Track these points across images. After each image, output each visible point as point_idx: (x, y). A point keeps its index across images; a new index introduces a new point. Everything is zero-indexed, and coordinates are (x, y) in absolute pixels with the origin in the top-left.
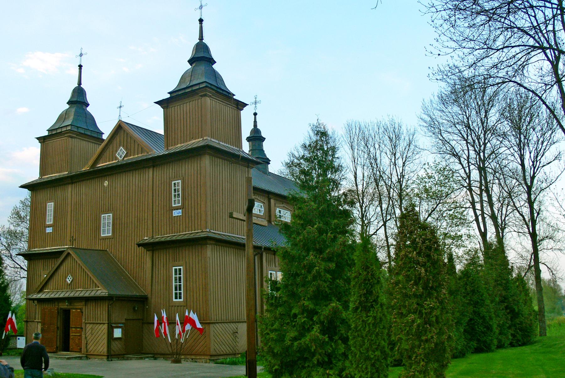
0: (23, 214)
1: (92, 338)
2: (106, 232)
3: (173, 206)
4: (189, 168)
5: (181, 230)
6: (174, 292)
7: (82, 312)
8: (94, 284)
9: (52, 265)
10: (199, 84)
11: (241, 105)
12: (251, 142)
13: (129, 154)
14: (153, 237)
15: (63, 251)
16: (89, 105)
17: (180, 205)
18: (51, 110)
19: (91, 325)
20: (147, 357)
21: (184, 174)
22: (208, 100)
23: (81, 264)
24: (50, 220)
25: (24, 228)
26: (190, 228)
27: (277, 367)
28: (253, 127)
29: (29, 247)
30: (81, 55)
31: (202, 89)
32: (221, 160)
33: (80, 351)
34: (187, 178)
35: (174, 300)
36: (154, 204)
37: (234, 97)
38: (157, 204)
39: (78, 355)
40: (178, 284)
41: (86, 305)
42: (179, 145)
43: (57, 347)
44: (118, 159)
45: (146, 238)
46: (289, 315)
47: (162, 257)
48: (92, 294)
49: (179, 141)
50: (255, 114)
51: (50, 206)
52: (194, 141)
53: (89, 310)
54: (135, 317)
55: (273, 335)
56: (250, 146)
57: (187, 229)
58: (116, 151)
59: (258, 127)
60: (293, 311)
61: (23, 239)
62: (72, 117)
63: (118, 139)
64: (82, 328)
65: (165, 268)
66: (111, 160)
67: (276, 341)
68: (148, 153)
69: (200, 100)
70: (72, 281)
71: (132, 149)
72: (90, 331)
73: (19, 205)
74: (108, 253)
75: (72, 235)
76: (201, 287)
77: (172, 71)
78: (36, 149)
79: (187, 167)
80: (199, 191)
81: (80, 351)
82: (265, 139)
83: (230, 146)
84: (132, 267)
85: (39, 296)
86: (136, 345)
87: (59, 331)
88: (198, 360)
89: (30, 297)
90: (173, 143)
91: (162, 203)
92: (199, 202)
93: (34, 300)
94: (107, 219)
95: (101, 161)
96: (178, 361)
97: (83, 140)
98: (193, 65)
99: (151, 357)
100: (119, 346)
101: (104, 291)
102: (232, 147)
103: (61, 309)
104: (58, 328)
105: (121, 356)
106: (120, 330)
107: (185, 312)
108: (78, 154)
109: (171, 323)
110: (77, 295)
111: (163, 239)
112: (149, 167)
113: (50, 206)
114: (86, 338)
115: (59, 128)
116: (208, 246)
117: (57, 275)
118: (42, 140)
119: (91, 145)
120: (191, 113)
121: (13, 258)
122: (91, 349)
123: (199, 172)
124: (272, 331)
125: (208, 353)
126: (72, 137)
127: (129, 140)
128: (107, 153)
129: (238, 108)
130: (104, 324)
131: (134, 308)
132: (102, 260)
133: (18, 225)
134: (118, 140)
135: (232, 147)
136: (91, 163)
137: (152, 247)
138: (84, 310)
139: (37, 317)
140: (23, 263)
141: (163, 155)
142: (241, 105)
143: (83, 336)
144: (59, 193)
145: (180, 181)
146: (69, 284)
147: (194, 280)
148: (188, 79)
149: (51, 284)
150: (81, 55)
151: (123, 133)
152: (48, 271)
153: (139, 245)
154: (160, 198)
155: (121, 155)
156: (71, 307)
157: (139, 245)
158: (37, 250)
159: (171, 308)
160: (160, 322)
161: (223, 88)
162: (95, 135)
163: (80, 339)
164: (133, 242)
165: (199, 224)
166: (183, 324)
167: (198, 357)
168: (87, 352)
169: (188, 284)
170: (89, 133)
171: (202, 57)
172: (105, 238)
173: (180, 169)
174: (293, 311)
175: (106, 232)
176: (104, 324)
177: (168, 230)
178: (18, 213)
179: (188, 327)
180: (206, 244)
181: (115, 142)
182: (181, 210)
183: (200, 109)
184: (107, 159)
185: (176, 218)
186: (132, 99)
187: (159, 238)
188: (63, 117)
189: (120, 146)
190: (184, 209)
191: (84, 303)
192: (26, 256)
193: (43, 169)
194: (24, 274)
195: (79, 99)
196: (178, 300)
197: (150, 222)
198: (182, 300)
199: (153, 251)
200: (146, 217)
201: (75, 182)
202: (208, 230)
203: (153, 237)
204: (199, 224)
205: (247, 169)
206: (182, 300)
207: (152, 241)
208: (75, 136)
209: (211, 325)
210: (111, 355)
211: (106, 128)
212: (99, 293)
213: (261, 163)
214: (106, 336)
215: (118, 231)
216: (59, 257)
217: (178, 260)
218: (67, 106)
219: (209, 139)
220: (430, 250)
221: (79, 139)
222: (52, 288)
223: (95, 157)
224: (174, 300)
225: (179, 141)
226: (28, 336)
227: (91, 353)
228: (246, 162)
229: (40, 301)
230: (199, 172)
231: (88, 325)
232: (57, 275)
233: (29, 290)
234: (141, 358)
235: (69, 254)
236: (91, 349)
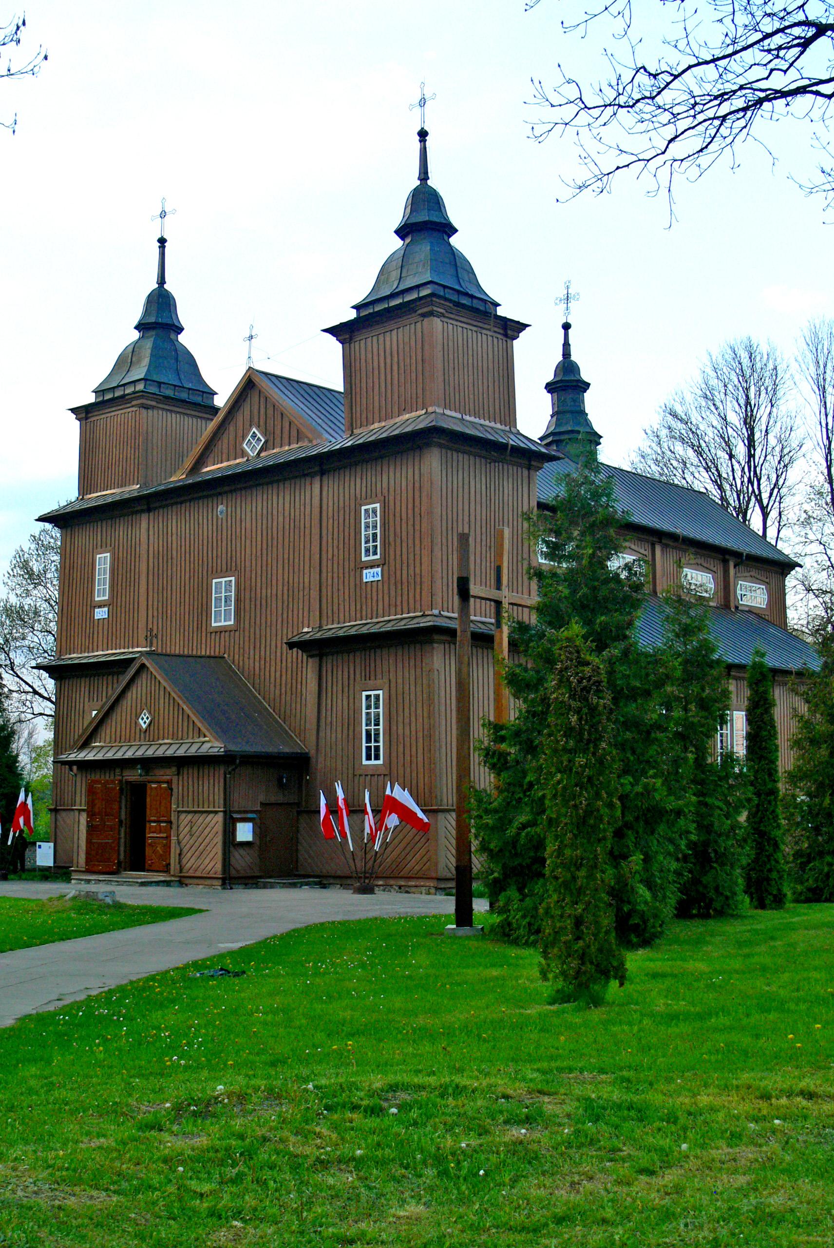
0: (36, 567)
1: (191, 842)
2: (222, 617)
3: (364, 559)
4: (396, 476)
5: (380, 612)
6: (364, 745)
7: (172, 790)
8: (196, 731)
9: (109, 689)
10: (418, 287)
11: (512, 329)
12: (555, 395)
13: (271, 443)
14: (320, 627)
15: (133, 659)
16: (182, 329)
17: (378, 557)
18: (100, 345)
19: (190, 817)
20: (307, 884)
21: (385, 492)
22: (437, 322)
23: (168, 689)
24: (102, 592)
25: (43, 598)
26: (399, 609)
27: (496, 875)
28: (561, 358)
29: (60, 652)
30: (163, 215)
31: (429, 294)
32: (466, 456)
33: (166, 869)
34: (391, 498)
35: (365, 762)
36: (324, 553)
37: (500, 312)
38: (330, 556)
39: (161, 877)
40: (373, 727)
41: (178, 774)
42: (376, 425)
43: (119, 863)
44: (247, 455)
45: (306, 630)
46: (521, 786)
47: (341, 670)
48: (192, 751)
49: (377, 416)
50: (566, 327)
51: (103, 560)
52: (407, 416)
53: (184, 786)
54: (280, 799)
55: (489, 820)
56: (553, 405)
57: (393, 610)
58: (243, 440)
59: (573, 358)
60: (528, 779)
61: (37, 626)
62: (146, 361)
63: (246, 409)
64: (170, 822)
65: (346, 694)
66: (232, 455)
67: (493, 829)
68: (310, 441)
69: (419, 325)
70: (150, 725)
71: (278, 432)
72: (187, 829)
73: (28, 546)
74: (226, 662)
75: (150, 626)
76: (420, 734)
77: (359, 258)
78: (71, 430)
79: (392, 474)
80: (417, 527)
81: (166, 869)
82: (588, 385)
83: (487, 423)
84: (277, 692)
85: (82, 756)
86: (280, 859)
87: (123, 830)
88: (413, 889)
89: (63, 757)
90: (364, 420)
91: (341, 552)
92: (418, 552)
93: (71, 764)
94: (223, 587)
95: (210, 460)
96: (367, 890)
97: (171, 411)
98: (408, 240)
99: (316, 884)
100: (248, 859)
101: (217, 744)
102: (492, 424)
103: (127, 782)
104: (121, 822)
105: (250, 881)
106: (249, 826)
107: (385, 788)
108: (163, 441)
109: (357, 811)
110: (160, 753)
111: (341, 633)
112: (312, 475)
113: (103, 560)
114: (179, 843)
115: (118, 386)
116: (435, 645)
117: (119, 711)
118: (82, 413)
119: (188, 422)
120: (401, 354)
121: (16, 669)
122: (189, 865)
123: (417, 485)
124: (487, 811)
125: (434, 875)
126: (147, 407)
127: (270, 411)
128: (224, 443)
129: (506, 335)
130: (216, 812)
131: (280, 780)
132: (211, 680)
133: (28, 593)
134: (247, 412)
135: (492, 424)
136: (188, 463)
137: (319, 649)
138: (174, 787)
139: (78, 799)
140: (49, 684)
141: (341, 450)
142: (512, 329)
143: (174, 839)
144: (121, 531)
145: (378, 505)
146: (146, 728)
147: (407, 721)
148: (395, 274)
149: (107, 731)
150: (163, 215)
151: (256, 399)
152: (100, 703)
153: (291, 645)
154: (335, 542)
155: (253, 448)
156: (149, 778)
157: (291, 645)
158: (75, 657)
159: (355, 779)
160: (333, 809)
161: (472, 291)
162: (195, 398)
163: (167, 847)
164: (279, 637)
165: (418, 597)
166: (380, 813)
167: (413, 883)
168: (181, 871)
169: (394, 728)
170: (184, 396)
171: (426, 221)
172: (221, 631)
173: (379, 478)
174: (528, 779)
175: (222, 617)
176: (216, 812)
177: (353, 614)
178: (25, 565)
179: (393, 820)
180: (431, 642)
181: (240, 417)
182: (379, 570)
183: (419, 346)
184: (224, 456)
185: (369, 585)
186: (274, 322)
187: (334, 629)
188: (126, 361)
189: (251, 426)
190: (386, 567)
191: (174, 769)
192: (53, 671)
193: (86, 481)
194: (49, 708)
195: (160, 318)
196: (373, 762)
197: (315, 594)
198: (380, 762)
199: (321, 656)
200: (307, 584)
201: (155, 509)
202: (436, 612)
203: (320, 627)
204: (418, 597)
205: (526, 472)
206: (380, 762)
207: (318, 636)
208: (154, 403)
209: (441, 816)
210: (231, 878)
211: (223, 385)
212: (205, 749)
213: (559, 459)
214: (219, 839)
215: (247, 614)
216: (124, 673)
217: (372, 678)
218: (136, 335)
219: (439, 410)
220: (588, 692)
221: (163, 409)
222: (108, 740)
223: (197, 450)
224: (365, 762)
225: (377, 416)
226: (59, 841)
227: (191, 874)
228: (528, 458)
229: (84, 765)
230: (417, 485)
231: (183, 816)
232: (118, 710)
233: (58, 744)
234: (294, 885)
235: (143, 666)
236: (189, 865)
